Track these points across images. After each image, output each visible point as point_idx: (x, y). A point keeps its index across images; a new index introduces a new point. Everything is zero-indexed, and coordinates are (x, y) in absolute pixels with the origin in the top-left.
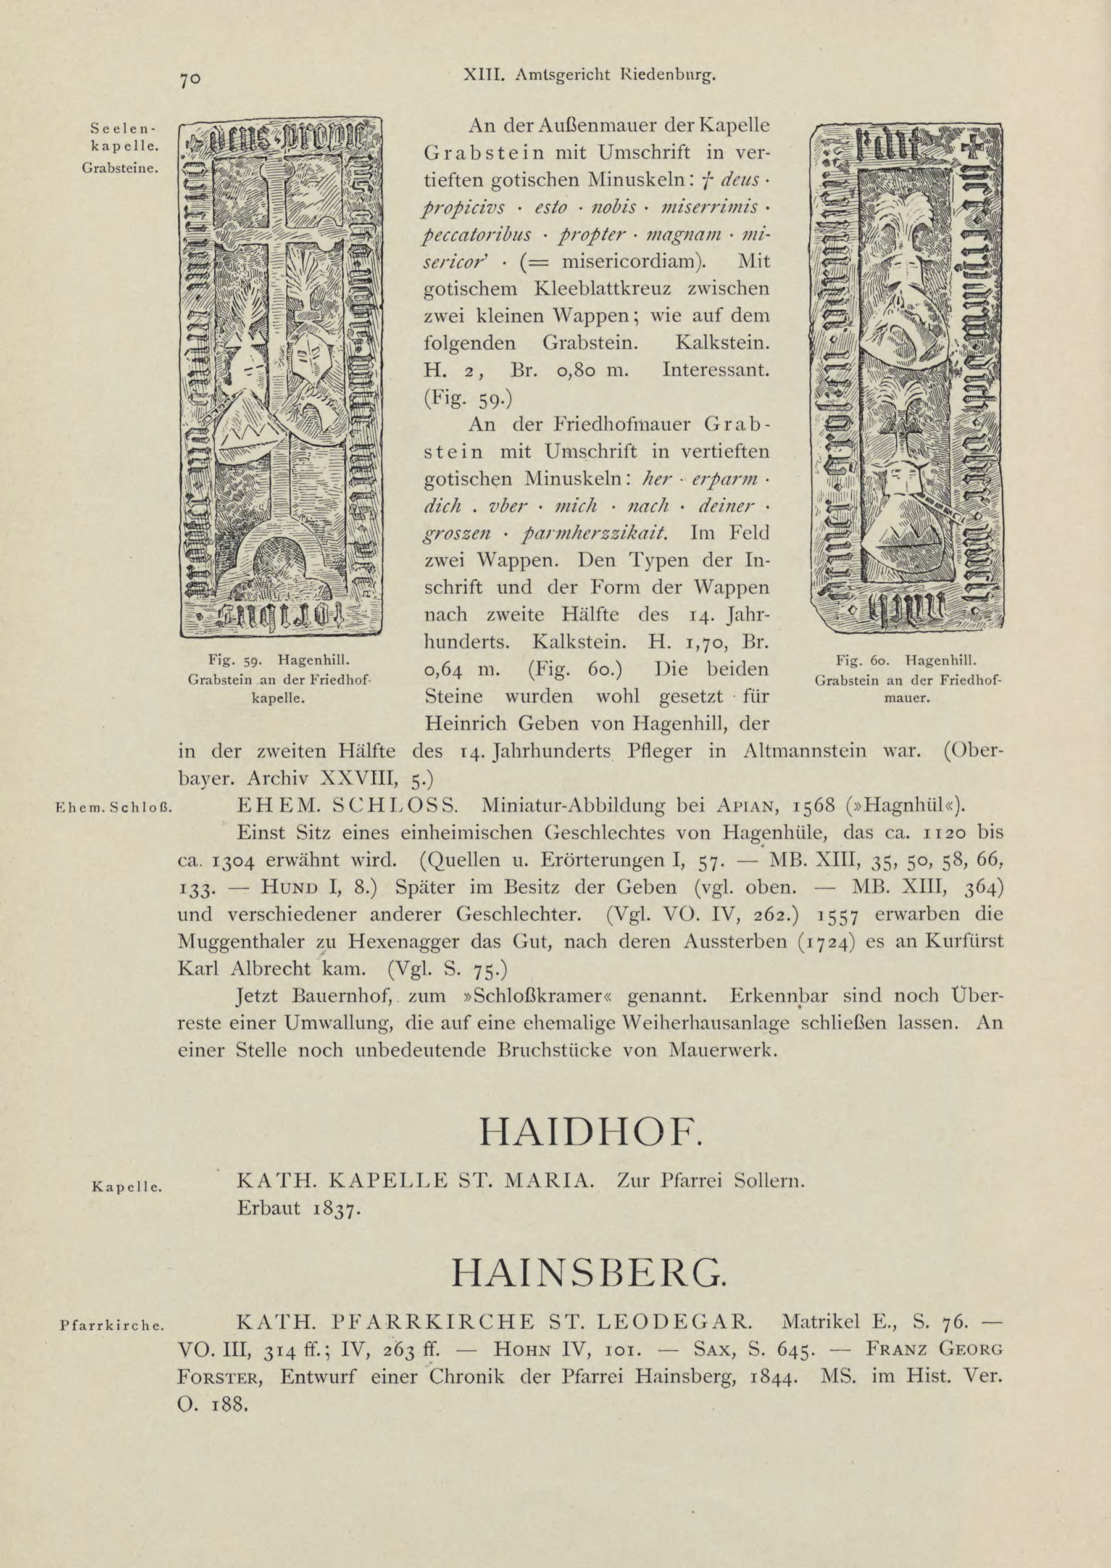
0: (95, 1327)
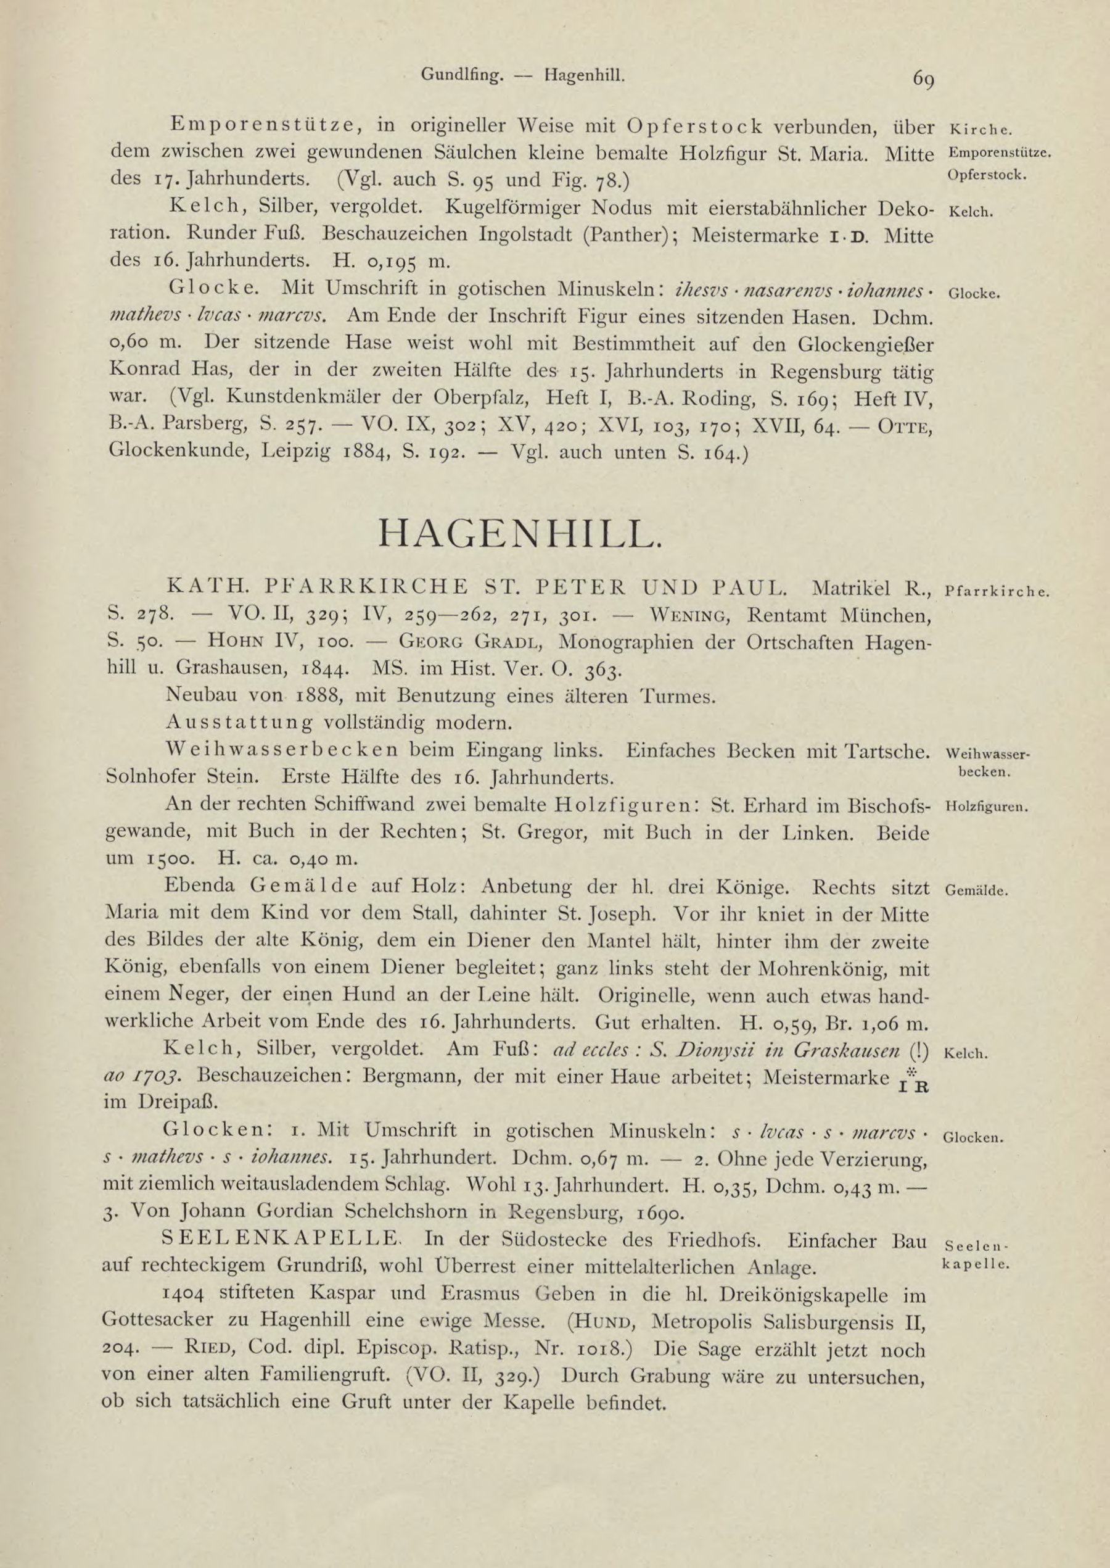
0: (980, 593)
